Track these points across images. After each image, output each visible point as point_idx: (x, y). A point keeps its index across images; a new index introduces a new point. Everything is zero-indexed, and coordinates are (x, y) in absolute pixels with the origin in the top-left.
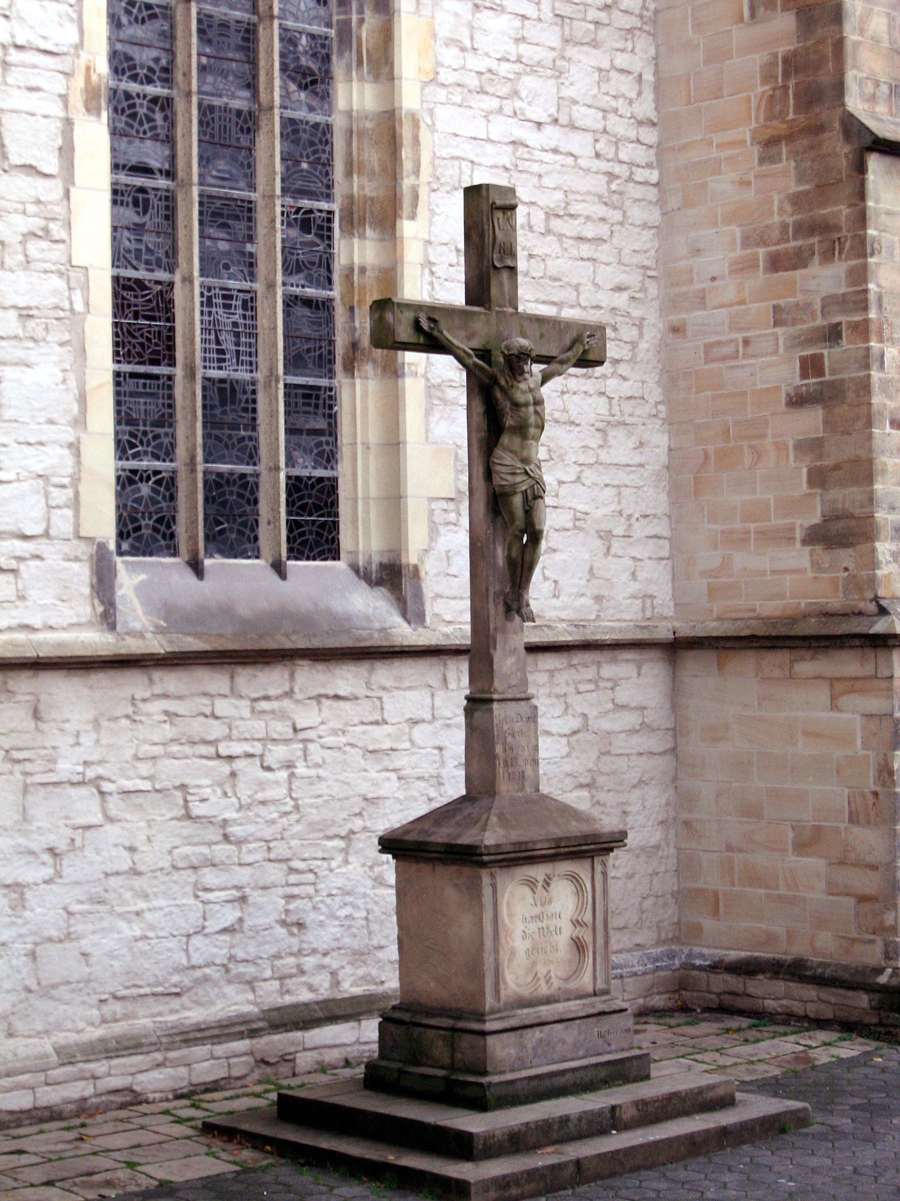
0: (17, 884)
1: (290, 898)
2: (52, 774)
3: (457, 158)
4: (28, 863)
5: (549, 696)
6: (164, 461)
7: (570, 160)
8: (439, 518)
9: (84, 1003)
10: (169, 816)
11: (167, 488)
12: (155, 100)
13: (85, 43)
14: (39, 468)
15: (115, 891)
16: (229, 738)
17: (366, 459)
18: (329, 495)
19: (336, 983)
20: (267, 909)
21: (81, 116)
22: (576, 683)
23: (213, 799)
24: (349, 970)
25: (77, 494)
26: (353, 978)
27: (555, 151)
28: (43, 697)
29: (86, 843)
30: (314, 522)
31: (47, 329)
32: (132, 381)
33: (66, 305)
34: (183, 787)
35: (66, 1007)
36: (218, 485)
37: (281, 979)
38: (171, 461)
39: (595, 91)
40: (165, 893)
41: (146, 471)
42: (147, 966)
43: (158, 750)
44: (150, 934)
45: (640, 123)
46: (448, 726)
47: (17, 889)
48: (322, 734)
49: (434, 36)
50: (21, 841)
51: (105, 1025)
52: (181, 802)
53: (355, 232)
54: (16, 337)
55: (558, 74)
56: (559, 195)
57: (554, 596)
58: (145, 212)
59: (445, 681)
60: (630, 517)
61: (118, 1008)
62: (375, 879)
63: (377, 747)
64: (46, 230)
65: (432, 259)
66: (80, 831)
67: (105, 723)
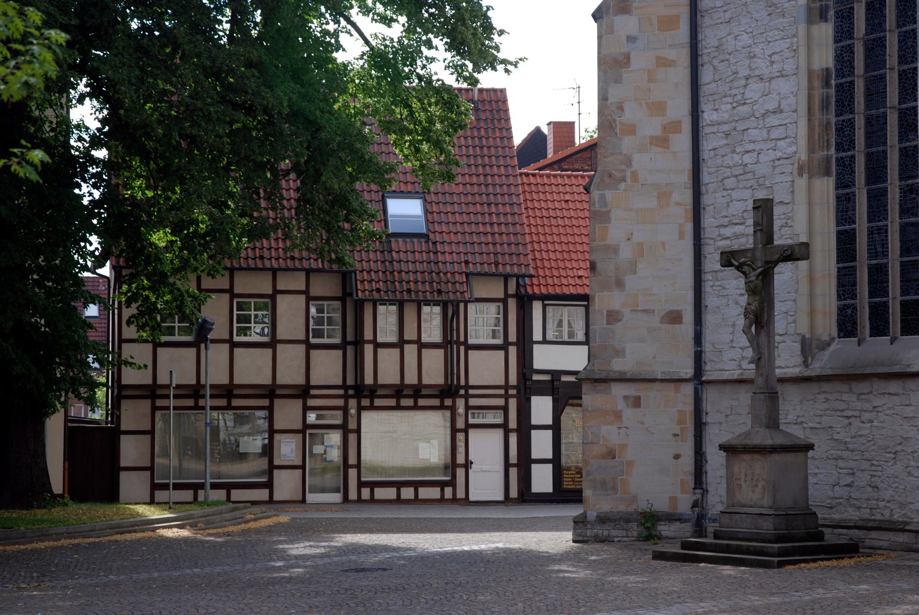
1: (872, 476)
14: (784, 310)
16: (848, 409)
19: (891, 515)
20: (863, 479)
24: (898, 510)
36: (844, 309)
37: (871, 509)
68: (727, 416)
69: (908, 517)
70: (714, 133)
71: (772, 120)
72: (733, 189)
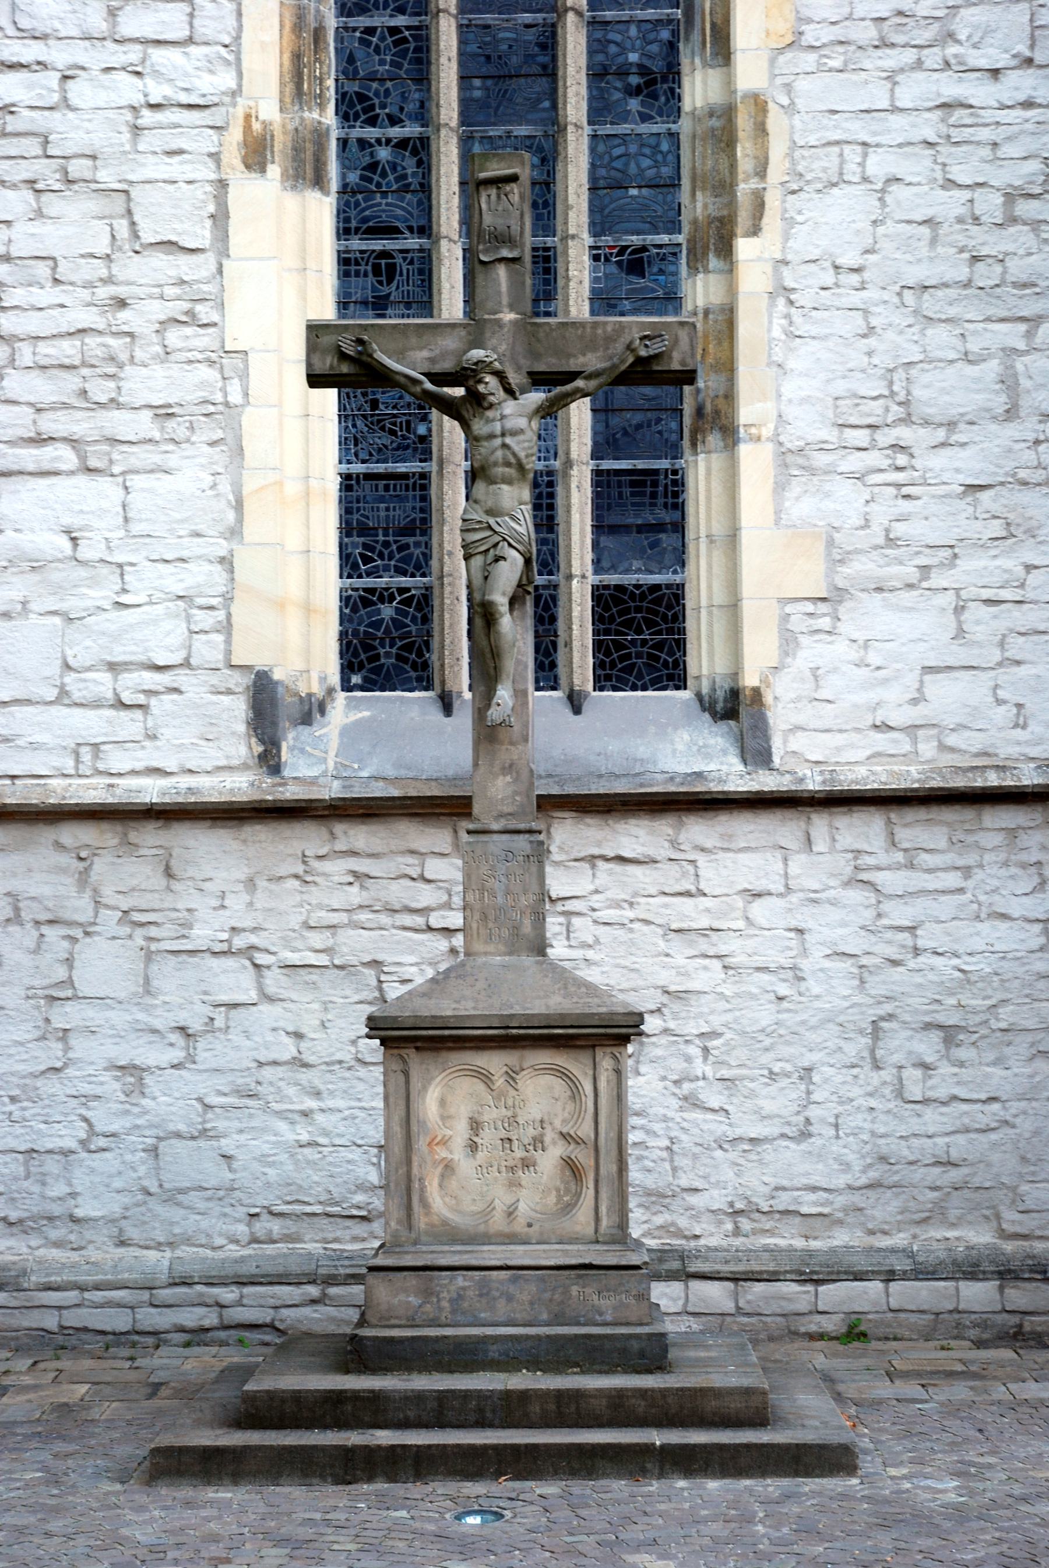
0: (135, 1067)
2: (184, 941)
3: (837, 143)
4: (150, 1043)
5: (1006, 864)
6: (413, 576)
8: (797, 623)
9: (225, 1215)
10: (356, 998)
11: (419, 608)
12: (403, 144)
13: (244, 89)
15: (271, 1083)
17: (709, 556)
18: (670, 607)
21: (239, 175)
25: (229, 615)
26: (646, 1226)
27: (1028, 104)
28: (175, 852)
29: (231, 1024)
30: (644, 642)
31: (192, 428)
32: (367, 485)
34: (375, 964)
35: (198, 1217)
36: (366, 603)
38: (424, 575)
40: (345, 1092)
41: (387, 589)
42: (316, 1178)
43: (342, 918)
44: (321, 1140)
46: (814, 901)
47: (133, 1071)
48: (596, 906)
50: (141, 1016)
51: (256, 1246)
52: (374, 983)
53: (699, 266)
57: (1016, 726)
58: (390, 281)
61: (276, 1227)
62: (685, 1098)
63: (684, 925)
65: (790, 283)
66: (223, 1009)
67: (262, 883)
69: (679, 1234)
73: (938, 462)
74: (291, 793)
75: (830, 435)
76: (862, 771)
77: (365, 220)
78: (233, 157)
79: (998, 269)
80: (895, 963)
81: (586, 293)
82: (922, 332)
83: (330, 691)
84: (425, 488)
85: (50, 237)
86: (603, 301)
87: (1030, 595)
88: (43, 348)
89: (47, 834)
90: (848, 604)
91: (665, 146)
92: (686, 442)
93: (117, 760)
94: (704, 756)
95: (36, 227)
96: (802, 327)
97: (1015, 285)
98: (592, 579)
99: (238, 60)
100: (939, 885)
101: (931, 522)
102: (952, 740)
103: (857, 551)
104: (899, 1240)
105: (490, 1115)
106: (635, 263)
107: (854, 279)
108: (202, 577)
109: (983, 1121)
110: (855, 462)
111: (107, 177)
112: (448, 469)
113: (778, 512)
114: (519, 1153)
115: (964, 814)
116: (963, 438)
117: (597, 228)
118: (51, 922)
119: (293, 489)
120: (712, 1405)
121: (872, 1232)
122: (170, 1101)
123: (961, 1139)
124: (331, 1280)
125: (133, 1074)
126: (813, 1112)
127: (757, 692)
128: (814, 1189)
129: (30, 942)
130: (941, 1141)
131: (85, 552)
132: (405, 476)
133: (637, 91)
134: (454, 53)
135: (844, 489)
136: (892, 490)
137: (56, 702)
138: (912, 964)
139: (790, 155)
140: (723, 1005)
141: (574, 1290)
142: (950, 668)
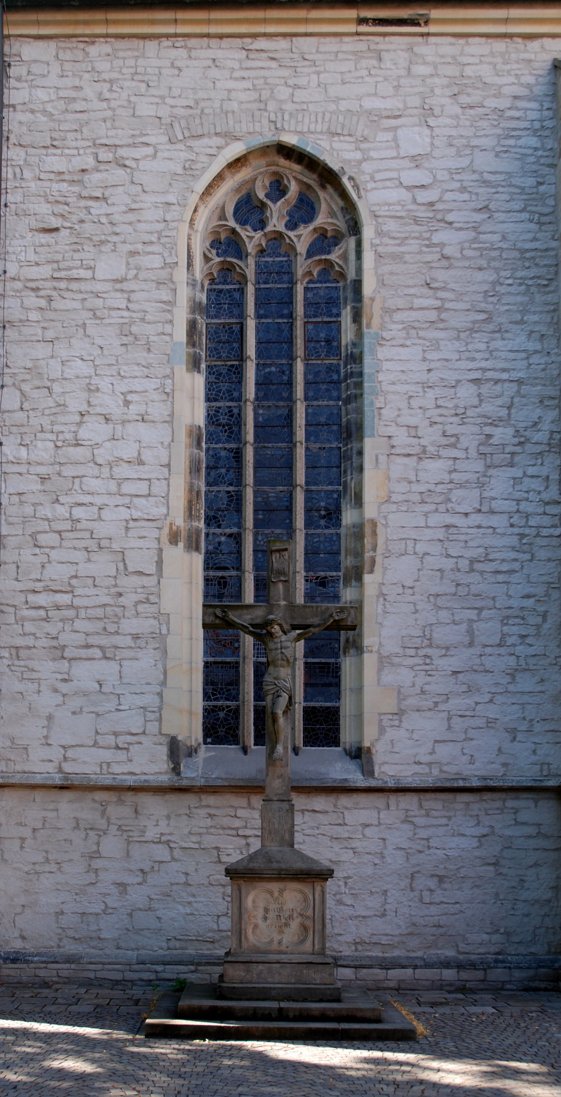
5: (465, 815)
7: (490, 531)
8: (385, 723)
12: (230, 535)
16: (246, 827)
18: (334, 715)
22: (486, 810)
23: (234, 855)
25: (161, 715)
27: (479, 527)
31: (147, 643)
33: (158, 631)
34: (217, 848)
36: (213, 711)
39: (510, 490)
45: (547, 503)
49: (389, 479)
50: (126, 865)
54: (131, 647)
55: (481, 485)
56: (481, 550)
59: (388, 806)
60: (531, 720)
61: (178, 944)
64: (147, 599)
65: (385, 592)
68: (34, 830)
70: (20, 474)
71: (123, 471)
72: (53, 548)
73: (442, 662)
74: (185, 783)
75: (400, 651)
76: (410, 779)
77: (215, 564)
78: (165, 539)
79: (467, 589)
80: (420, 852)
81: (303, 594)
82: (437, 612)
83: (199, 744)
84: (238, 667)
85: (92, 569)
86: (309, 596)
87: (477, 714)
88: (89, 611)
89: (89, 796)
90: (406, 716)
91: (335, 538)
92: (341, 652)
93: (116, 769)
94: (349, 773)
95: (89, 565)
96: (389, 608)
97: (474, 595)
98: (303, 704)
99: (168, 502)
100: (439, 823)
101: (438, 685)
102: (445, 768)
103: (410, 696)
104: (419, 954)
105: (272, 906)
106: (323, 582)
107: (410, 591)
108: (150, 700)
109: (452, 911)
110: (410, 661)
111: (115, 546)
112: (247, 661)
113: (379, 680)
114: (283, 921)
115: (449, 796)
116: (452, 653)
117: (307, 569)
118: (91, 829)
119: (186, 667)
120: (359, 1014)
121: (408, 951)
122: (137, 896)
123: (444, 917)
124: (199, 964)
125: (123, 887)
126: (387, 907)
127: (369, 749)
128: (387, 935)
129: (83, 836)
130: (437, 918)
131: (104, 689)
132: (229, 663)
133: (324, 517)
134: (252, 501)
135: (405, 671)
136: (424, 673)
137: (94, 746)
138: (427, 852)
139: (386, 543)
140: (353, 866)
141: (305, 971)
142: (445, 741)
